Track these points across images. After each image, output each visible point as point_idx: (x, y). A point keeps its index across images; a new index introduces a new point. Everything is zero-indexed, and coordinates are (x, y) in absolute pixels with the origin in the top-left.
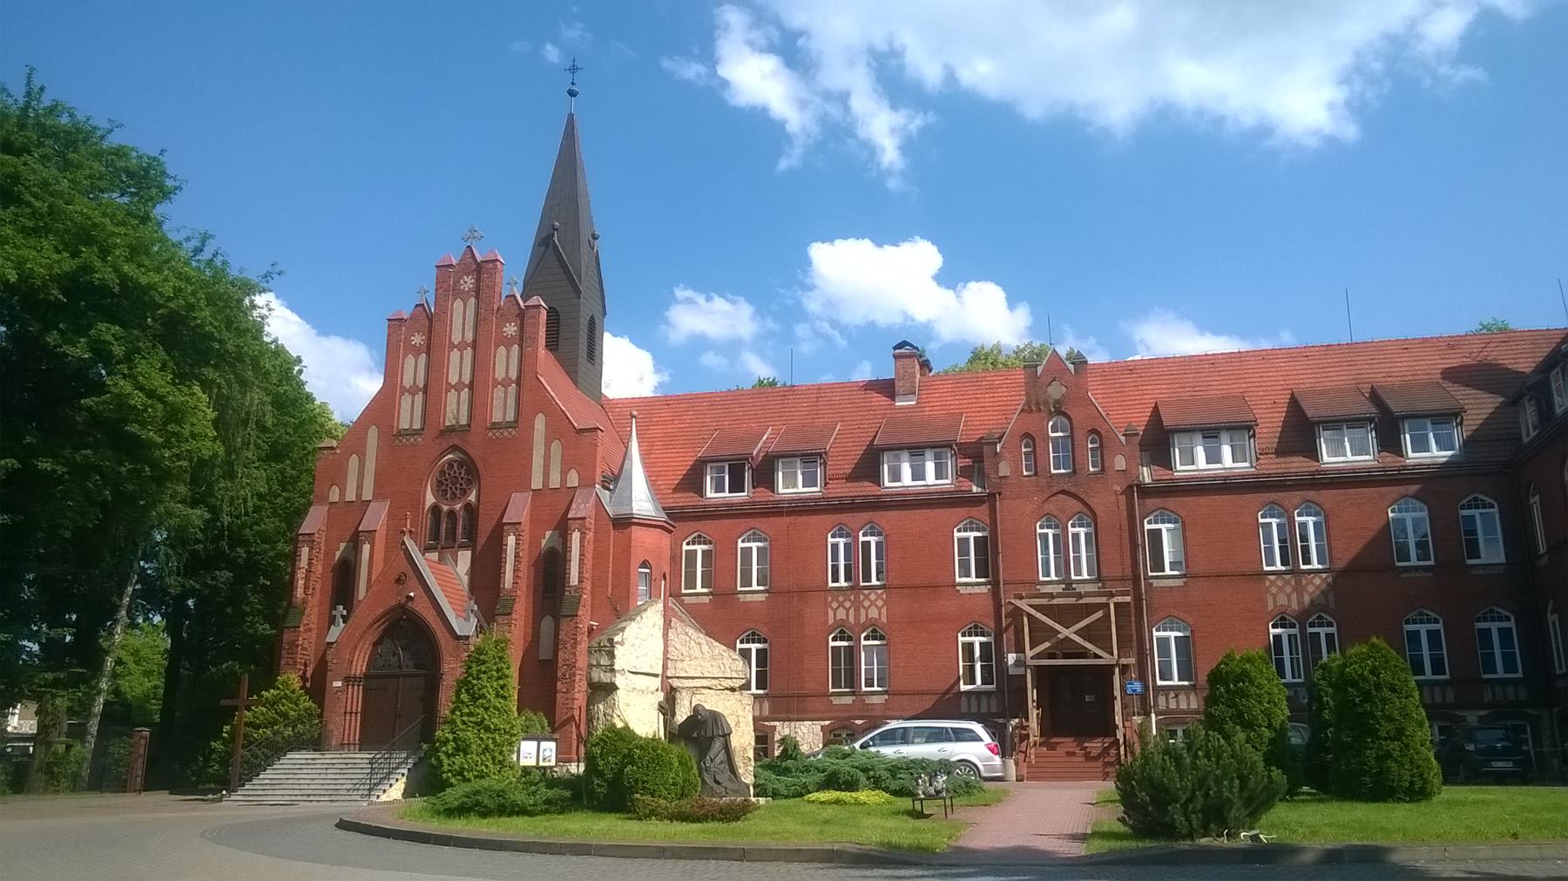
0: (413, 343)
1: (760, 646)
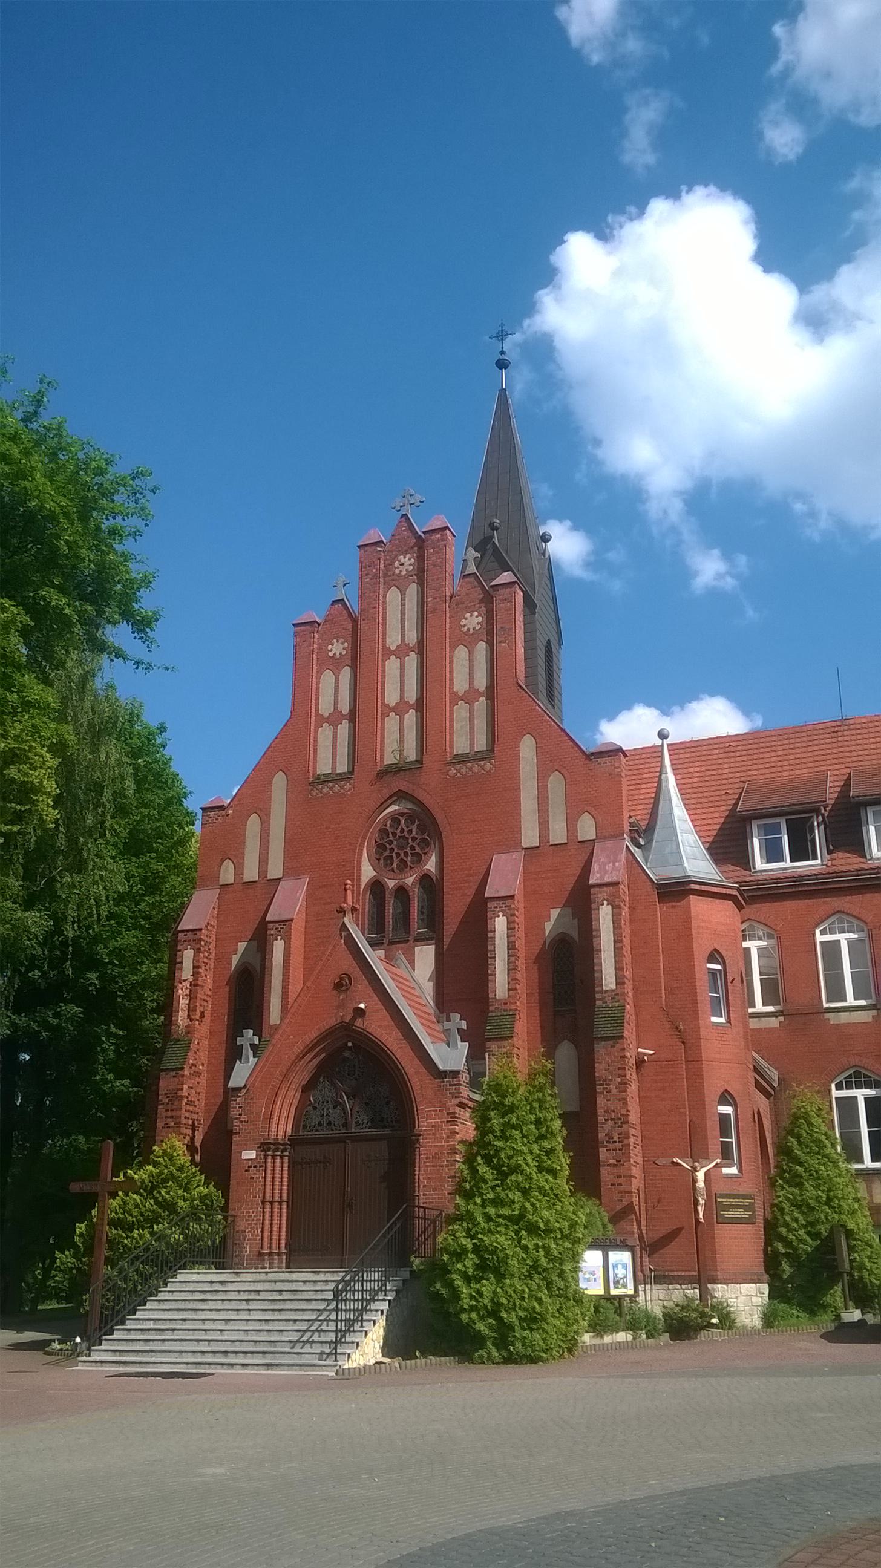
0: (331, 654)
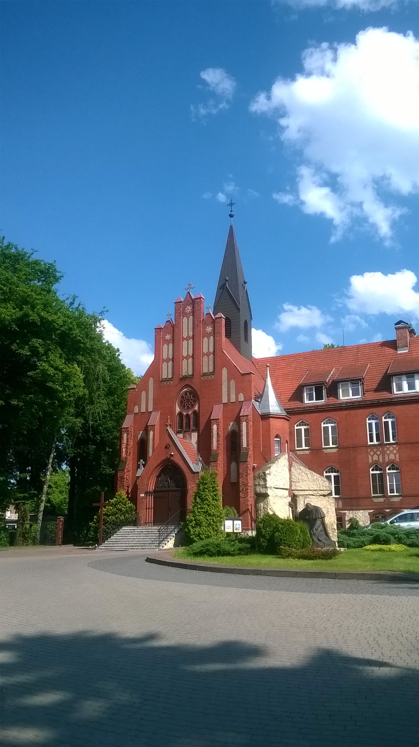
0: (166, 339)
1: (335, 474)
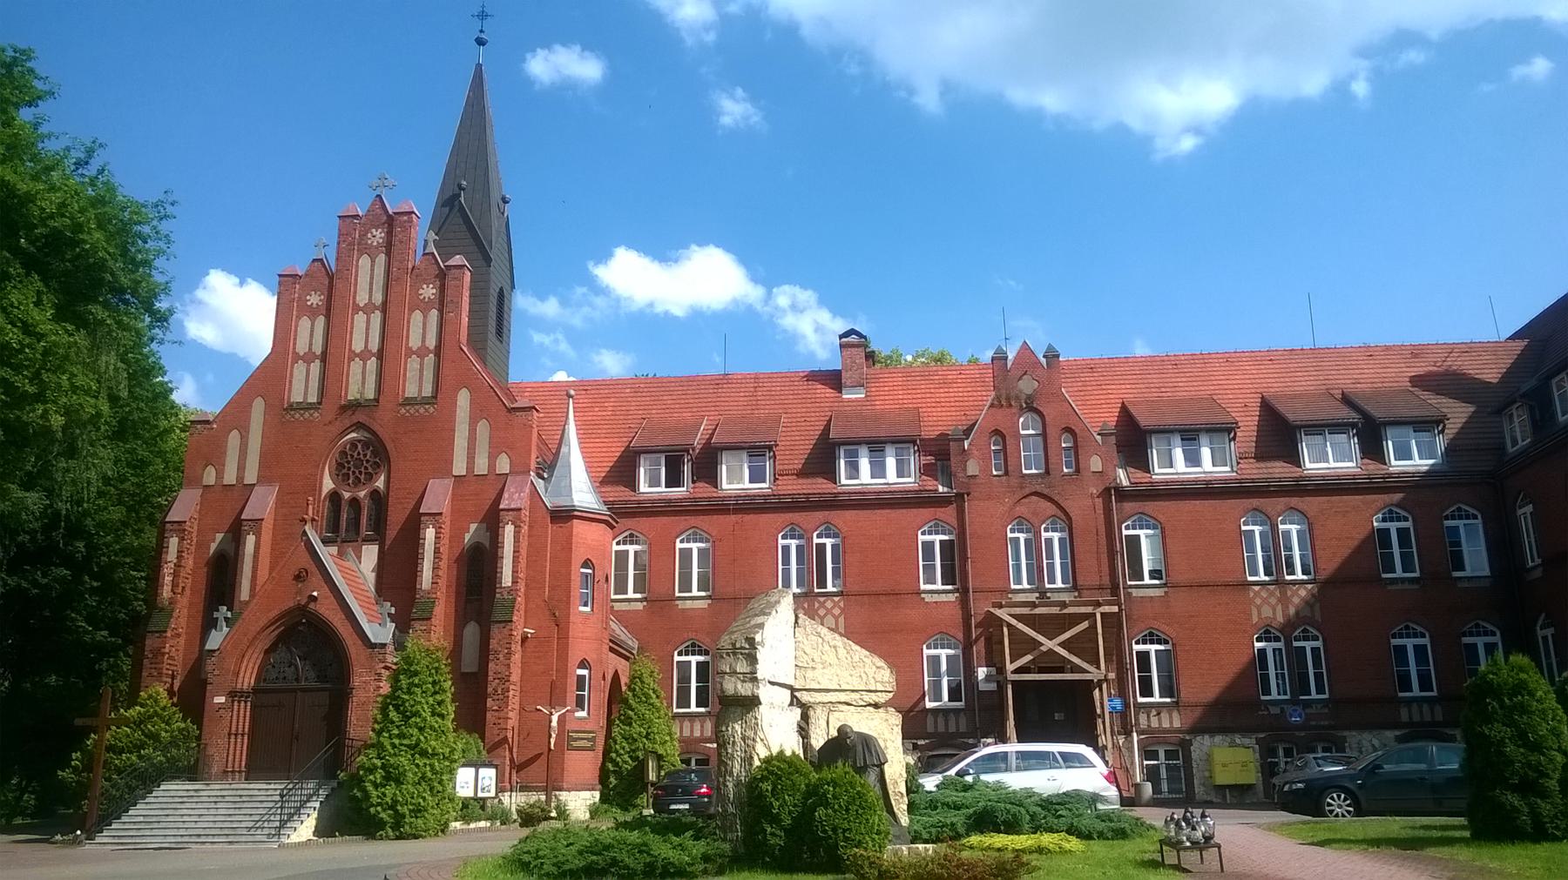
0: (309, 303)
1: (701, 658)
